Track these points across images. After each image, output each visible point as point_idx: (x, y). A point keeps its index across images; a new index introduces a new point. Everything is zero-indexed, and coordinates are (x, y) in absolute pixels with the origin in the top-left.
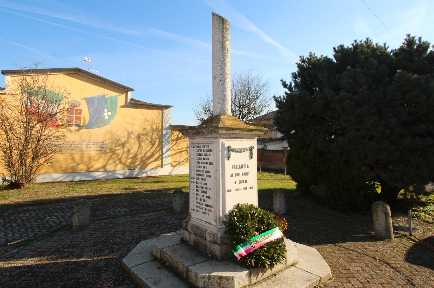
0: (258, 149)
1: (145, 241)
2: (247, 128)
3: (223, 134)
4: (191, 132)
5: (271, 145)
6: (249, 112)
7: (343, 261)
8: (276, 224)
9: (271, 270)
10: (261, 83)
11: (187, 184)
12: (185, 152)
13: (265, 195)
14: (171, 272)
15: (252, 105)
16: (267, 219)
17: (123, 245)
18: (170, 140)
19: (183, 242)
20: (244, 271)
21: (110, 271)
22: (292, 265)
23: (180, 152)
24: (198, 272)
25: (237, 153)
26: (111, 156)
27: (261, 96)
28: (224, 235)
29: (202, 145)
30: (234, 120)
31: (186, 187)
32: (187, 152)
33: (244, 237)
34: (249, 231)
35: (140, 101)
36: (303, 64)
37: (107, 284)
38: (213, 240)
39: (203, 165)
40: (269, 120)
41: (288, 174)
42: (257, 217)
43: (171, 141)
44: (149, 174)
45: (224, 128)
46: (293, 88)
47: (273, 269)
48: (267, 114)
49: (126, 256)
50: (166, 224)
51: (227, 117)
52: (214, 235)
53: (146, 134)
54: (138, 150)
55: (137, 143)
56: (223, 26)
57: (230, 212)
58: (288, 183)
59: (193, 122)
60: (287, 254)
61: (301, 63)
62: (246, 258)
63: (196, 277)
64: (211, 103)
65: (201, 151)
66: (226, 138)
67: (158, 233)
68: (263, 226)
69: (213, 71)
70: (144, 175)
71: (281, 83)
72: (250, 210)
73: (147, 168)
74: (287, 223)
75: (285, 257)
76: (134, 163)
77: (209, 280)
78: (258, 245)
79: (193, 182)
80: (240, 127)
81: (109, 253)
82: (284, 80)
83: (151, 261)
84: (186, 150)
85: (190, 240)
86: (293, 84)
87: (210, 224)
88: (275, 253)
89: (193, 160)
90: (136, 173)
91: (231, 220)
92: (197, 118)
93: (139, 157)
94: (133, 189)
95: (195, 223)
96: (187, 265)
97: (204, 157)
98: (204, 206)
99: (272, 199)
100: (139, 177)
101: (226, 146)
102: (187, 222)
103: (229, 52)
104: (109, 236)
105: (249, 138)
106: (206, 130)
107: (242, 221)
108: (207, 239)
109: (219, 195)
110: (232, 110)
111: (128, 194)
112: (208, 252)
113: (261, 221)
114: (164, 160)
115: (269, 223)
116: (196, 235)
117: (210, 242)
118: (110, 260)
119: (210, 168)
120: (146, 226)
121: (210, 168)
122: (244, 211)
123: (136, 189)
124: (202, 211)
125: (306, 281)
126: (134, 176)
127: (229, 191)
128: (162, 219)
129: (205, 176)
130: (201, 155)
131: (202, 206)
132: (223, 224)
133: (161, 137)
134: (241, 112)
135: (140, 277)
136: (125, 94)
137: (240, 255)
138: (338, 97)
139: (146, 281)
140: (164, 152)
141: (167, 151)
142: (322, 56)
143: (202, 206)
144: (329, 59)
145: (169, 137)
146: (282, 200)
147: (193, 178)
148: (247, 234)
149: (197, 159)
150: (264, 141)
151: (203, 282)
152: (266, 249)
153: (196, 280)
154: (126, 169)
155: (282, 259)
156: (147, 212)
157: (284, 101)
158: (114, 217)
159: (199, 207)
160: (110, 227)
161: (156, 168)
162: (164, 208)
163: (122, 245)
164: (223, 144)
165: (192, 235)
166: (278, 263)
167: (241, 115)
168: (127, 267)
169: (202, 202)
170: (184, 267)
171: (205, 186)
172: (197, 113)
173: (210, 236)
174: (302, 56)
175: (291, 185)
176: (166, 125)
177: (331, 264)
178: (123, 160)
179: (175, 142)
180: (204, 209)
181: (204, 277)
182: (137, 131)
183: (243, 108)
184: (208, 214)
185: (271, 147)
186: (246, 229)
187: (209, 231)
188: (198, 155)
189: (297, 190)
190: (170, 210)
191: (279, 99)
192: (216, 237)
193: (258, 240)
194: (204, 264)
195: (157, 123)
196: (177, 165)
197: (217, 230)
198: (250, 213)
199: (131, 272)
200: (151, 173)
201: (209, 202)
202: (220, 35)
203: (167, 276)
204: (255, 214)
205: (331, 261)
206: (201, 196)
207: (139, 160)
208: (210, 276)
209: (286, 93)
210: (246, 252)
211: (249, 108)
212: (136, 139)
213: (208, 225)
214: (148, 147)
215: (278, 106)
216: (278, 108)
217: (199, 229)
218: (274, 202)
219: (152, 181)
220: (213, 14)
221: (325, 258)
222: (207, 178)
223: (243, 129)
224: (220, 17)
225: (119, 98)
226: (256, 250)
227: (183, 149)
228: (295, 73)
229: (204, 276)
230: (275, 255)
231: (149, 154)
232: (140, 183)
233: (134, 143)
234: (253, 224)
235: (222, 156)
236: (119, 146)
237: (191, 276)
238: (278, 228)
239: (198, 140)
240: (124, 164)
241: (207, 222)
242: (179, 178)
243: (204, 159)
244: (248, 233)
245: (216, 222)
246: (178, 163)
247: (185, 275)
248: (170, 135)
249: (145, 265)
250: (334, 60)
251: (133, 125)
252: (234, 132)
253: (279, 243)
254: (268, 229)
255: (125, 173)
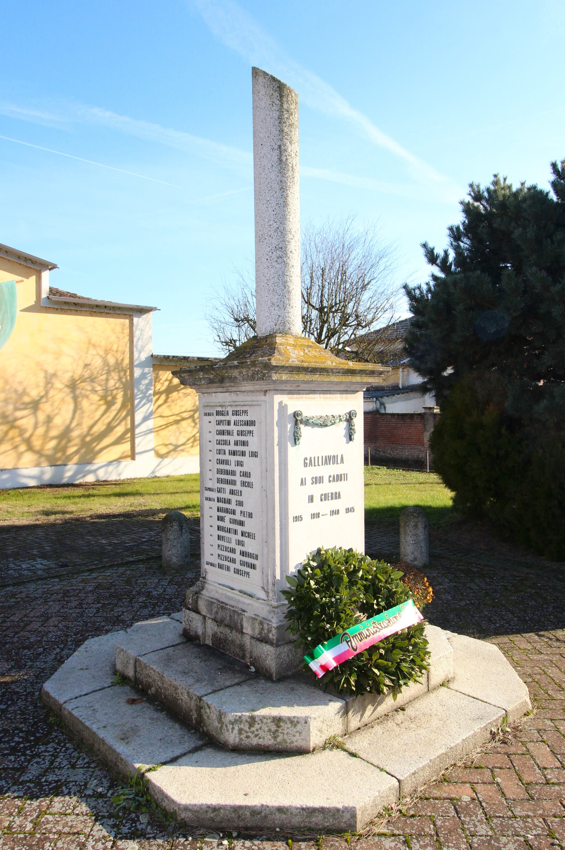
0: (365, 413)
1: (96, 639)
2: (342, 366)
3: (283, 382)
4: (204, 378)
5: (396, 402)
6: (344, 322)
7: (555, 670)
8: (406, 594)
9: (395, 699)
10: (375, 251)
11: (195, 499)
12: (190, 421)
13: (381, 524)
14: (161, 711)
15: (351, 305)
16: (386, 582)
17: (45, 649)
18: (151, 392)
19: (189, 638)
20: (332, 704)
21: (15, 711)
22: (442, 685)
23: (177, 422)
24: (224, 709)
25: (316, 429)
26: (6, 433)
27: (373, 282)
28: (285, 622)
29: (230, 410)
30: (309, 346)
31: (194, 507)
32: (194, 421)
33: (332, 625)
34: (343, 611)
35: (74, 296)
36: (476, 204)
37: (8, 742)
38: (260, 633)
39: (233, 459)
40: (391, 341)
41: (435, 469)
42: (362, 578)
43: (155, 394)
44: (102, 475)
45: (283, 368)
46: (451, 264)
47: (399, 696)
48: (388, 326)
49: (52, 674)
50: (148, 596)
51: (291, 341)
52: (261, 623)
53: (92, 379)
54: (73, 418)
55: (69, 399)
56: (282, 105)
57: (300, 568)
58: (434, 492)
59: (210, 348)
60: (432, 661)
61: (471, 201)
62: (337, 674)
63: (220, 720)
64: (253, 301)
65: (229, 423)
66: (290, 392)
67: (127, 617)
68: (377, 598)
69: (257, 223)
70: (90, 479)
71: (422, 251)
72: (347, 563)
73: (96, 461)
74: (431, 589)
75: (425, 669)
76: (64, 449)
77: (251, 725)
78: (365, 644)
79: (210, 499)
80: (322, 366)
81: (10, 670)
82: (431, 245)
83: (113, 684)
84: (192, 417)
85: (204, 633)
86: (452, 256)
87: (251, 596)
88: (404, 660)
89: (210, 446)
90: (68, 474)
91: (302, 586)
92: (217, 339)
93: (75, 434)
94: (64, 513)
95: (217, 596)
96: (198, 694)
97: (236, 437)
98: (237, 557)
99: (397, 533)
100: (77, 482)
101: (290, 411)
102: (197, 593)
103: (297, 175)
104: (8, 628)
105: (346, 392)
106: (241, 373)
107: (328, 588)
108: (244, 631)
109: (274, 529)
110: (303, 317)
111: (53, 525)
112: (248, 660)
113: (373, 588)
114: (137, 441)
115: (389, 590)
116: (219, 622)
117: (252, 637)
118: (13, 686)
119: (249, 463)
120: (99, 603)
121: (249, 463)
122: (333, 565)
123: (71, 512)
124: (232, 566)
125: (474, 720)
126: (65, 481)
127: (298, 519)
128: (136, 583)
129: (238, 483)
130: (229, 433)
131: (231, 555)
132: (283, 597)
133: (129, 387)
134: (323, 322)
135: (87, 724)
136: (33, 278)
137: (323, 667)
138: (558, 287)
139: (102, 734)
140: (137, 423)
141: (146, 419)
142: (523, 184)
143: (231, 555)
144: (541, 192)
145: (150, 384)
146: (421, 533)
147: (210, 489)
148: (339, 619)
149: (219, 443)
150: (379, 394)
151: (236, 731)
152: (382, 651)
153: (221, 728)
154: (45, 464)
155: (419, 674)
156: (100, 568)
157: (429, 295)
158: (20, 582)
159: (226, 558)
160: (10, 607)
161: (118, 460)
162: (141, 557)
163: (41, 650)
164: (283, 408)
165: (209, 623)
166: (411, 683)
167: (325, 330)
168: (55, 701)
169: (233, 545)
170: (191, 699)
171: (238, 509)
172: (216, 325)
173: (253, 624)
174: (476, 183)
175: (440, 496)
176: (142, 356)
177: (530, 680)
178: (37, 443)
179: (163, 397)
180: (238, 562)
181: (239, 720)
182: (67, 371)
183: (329, 315)
184: (248, 574)
185: (396, 406)
186: (337, 608)
187: (249, 614)
188: (222, 433)
189: (453, 509)
190: (155, 561)
191: (417, 292)
192: (266, 626)
193: (365, 632)
194: (238, 689)
195: (117, 351)
196: (168, 453)
197: (270, 612)
198: (346, 569)
199: (66, 713)
200: (106, 472)
201: (250, 546)
202: (273, 129)
203: (151, 719)
204: (358, 571)
205: (529, 671)
206: (229, 530)
207: (77, 441)
208: (253, 718)
209: (435, 278)
210: (336, 659)
211: (343, 312)
212: (67, 390)
213: (247, 600)
214: (97, 409)
215: (413, 309)
216: (414, 313)
217: (226, 609)
218: (402, 540)
219: (110, 492)
220: (256, 72)
221: (516, 665)
222: (245, 490)
223: (332, 369)
224: (274, 79)
225: (18, 286)
226: (360, 655)
227: (185, 415)
228: (458, 228)
229: (240, 717)
230: (404, 664)
231: (100, 427)
232: (80, 497)
233: (63, 400)
234: (354, 595)
235: (280, 437)
236: (25, 409)
237: (208, 717)
238: (410, 602)
239: (220, 397)
240: (39, 453)
241: (245, 593)
242: (175, 484)
243: (236, 443)
244: (343, 615)
245: (267, 593)
246: (171, 447)
247: (195, 716)
248: (151, 380)
249: (98, 695)
250: (553, 196)
251: (58, 355)
252: (308, 378)
253: (412, 637)
254: (389, 606)
255: (43, 473)
